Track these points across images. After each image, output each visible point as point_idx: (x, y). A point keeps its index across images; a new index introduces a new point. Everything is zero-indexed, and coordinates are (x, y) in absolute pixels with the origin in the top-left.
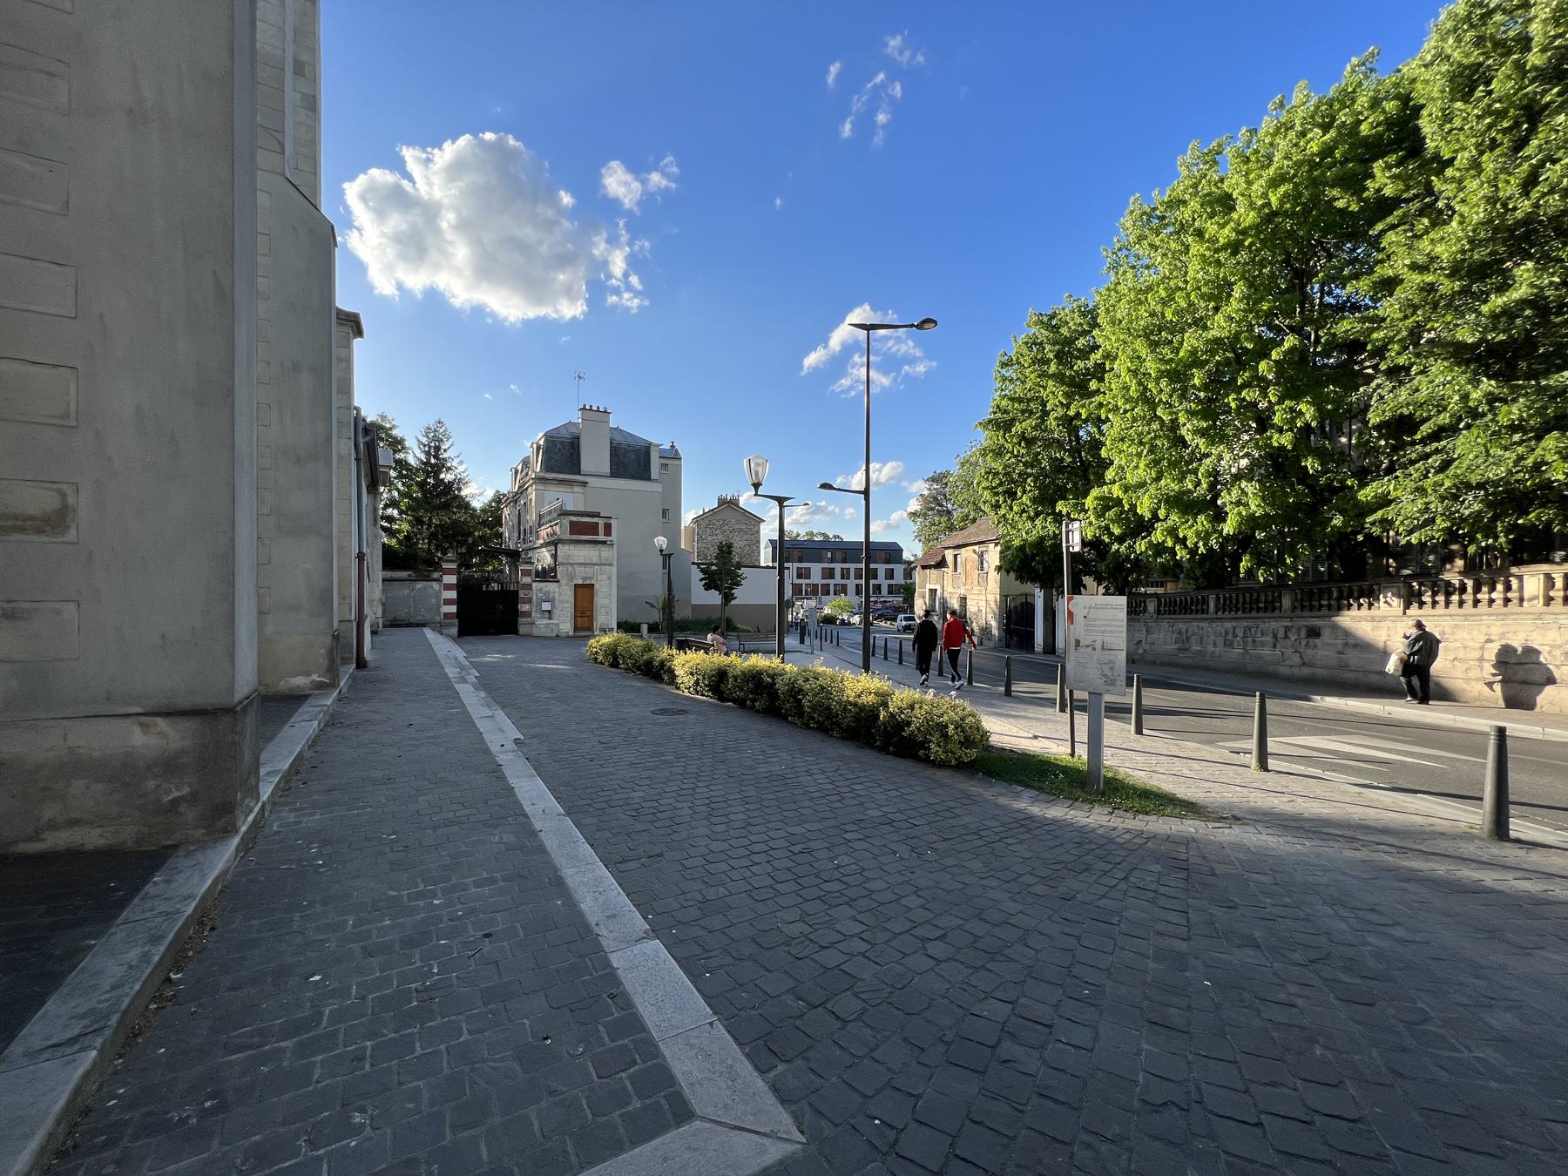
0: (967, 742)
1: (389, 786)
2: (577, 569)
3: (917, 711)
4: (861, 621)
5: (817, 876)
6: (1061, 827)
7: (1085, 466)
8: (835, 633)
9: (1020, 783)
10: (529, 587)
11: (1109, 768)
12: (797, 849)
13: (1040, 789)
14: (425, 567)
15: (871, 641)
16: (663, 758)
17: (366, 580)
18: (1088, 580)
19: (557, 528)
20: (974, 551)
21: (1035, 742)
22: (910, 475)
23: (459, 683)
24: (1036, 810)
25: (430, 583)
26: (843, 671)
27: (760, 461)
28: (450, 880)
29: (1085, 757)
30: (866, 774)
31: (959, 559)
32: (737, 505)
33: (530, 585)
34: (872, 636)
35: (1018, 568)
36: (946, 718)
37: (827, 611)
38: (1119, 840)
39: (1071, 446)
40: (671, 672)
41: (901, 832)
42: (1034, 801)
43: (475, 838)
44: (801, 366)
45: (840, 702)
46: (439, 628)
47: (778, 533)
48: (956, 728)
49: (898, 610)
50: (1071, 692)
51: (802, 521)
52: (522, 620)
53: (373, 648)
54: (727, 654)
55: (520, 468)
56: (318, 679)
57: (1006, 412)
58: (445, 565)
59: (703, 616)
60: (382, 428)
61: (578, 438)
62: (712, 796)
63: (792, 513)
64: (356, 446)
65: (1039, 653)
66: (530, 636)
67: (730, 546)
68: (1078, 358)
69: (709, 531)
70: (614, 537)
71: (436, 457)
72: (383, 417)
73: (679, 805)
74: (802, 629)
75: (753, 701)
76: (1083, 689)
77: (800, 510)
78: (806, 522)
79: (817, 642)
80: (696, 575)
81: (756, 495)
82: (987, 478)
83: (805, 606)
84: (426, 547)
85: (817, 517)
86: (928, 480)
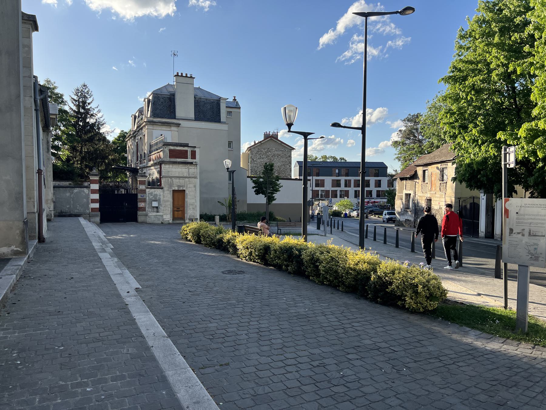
0: (431, 297)
1: (59, 317)
2: (174, 180)
3: (396, 275)
4: (358, 215)
5: (329, 382)
6: (497, 357)
7: (519, 109)
8: (340, 223)
9: (468, 325)
10: (144, 192)
11: (532, 317)
12: (315, 363)
13: (482, 330)
14: (79, 179)
15: (365, 228)
16: (229, 302)
17: (43, 186)
18: (518, 188)
19: (161, 154)
20: (438, 168)
21: (479, 298)
22: (391, 117)
23: (101, 252)
24: (479, 344)
25: (82, 189)
26: (346, 248)
27: (292, 108)
28: (97, 376)
29: (515, 309)
30: (361, 316)
31: (426, 173)
32: (277, 138)
33: (145, 191)
34: (365, 225)
35: (469, 179)
36: (416, 280)
37: (335, 208)
38: (538, 366)
39: (509, 94)
40: (234, 247)
41: (386, 355)
42: (478, 338)
43: (111, 350)
44: (318, 44)
45: (344, 268)
46: (89, 217)
47: (303, 157)
48: (424, 287)
49: (383, 208)
50: (506, 265)
51: (318, 148)
52: (139, 213)
53: (48, 230)
54: (270, 235)
55: (137, 115)
56: (16, 249)
57: (460, 70)
58: (92, 178)
59: (254, 211)
60: (49, 88)
61: (174, 95)
62: (261, 327)
63: (312, 144)
64: (35, 101)
65: (482, 238)
66: (144, 223)
67: (272, 166)
68: (514, 31)
69: (258, 156)
70: (197, 160)
71: (84, 108)
72: (48, 82)
73: (239, 333)
74: (319, 221)
75: (287, 266)
76: (515, 263)
77: (318, 141)
78: (321, 150)
79: (328, 229)
80: (250, 184)
81: (289, 131)
82: (447, 116)
83: (320, 205)
84: (79, 166)
85: (329, 146)
86: (404, 120)
